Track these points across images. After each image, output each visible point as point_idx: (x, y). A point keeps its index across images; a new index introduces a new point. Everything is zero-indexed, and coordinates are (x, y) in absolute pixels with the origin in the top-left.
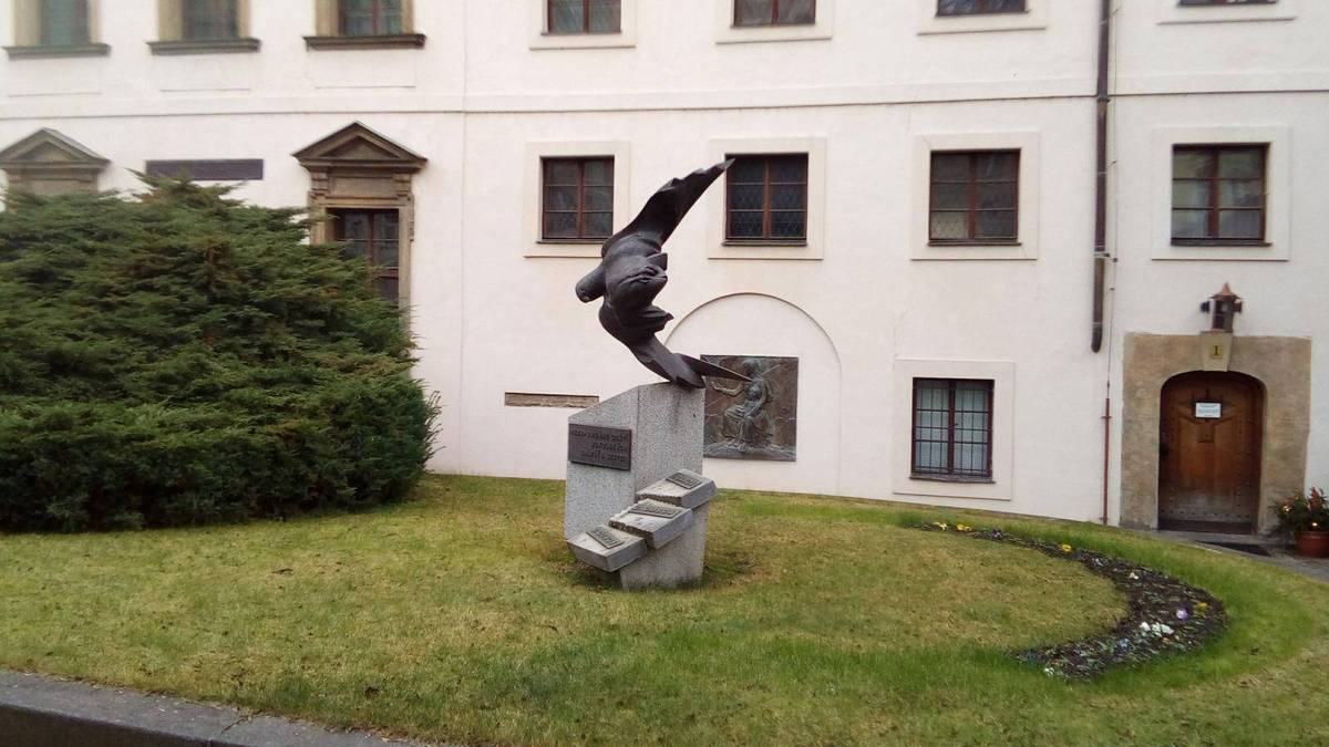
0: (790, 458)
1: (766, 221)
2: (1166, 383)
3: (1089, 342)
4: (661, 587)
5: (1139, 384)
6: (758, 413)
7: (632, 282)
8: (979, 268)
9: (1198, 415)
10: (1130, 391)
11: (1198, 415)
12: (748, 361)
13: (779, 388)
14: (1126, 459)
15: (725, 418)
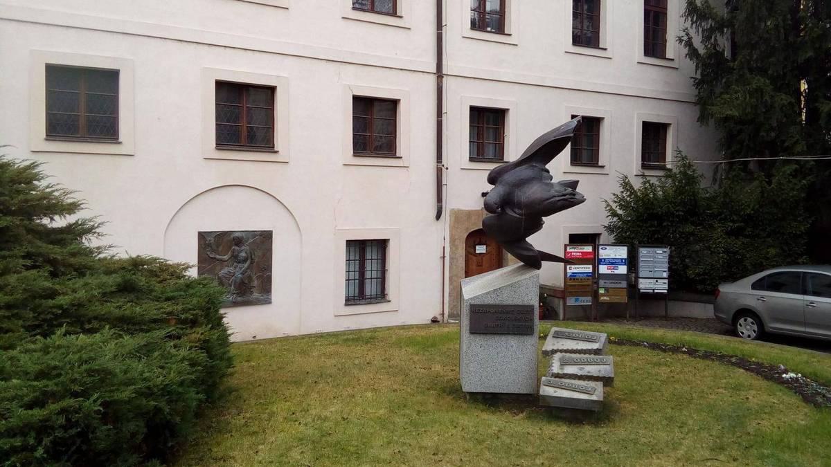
0: (269, 302)
1: (82, 122)
2: (467, 237)
3: (434, 213)
4: (561, 351)
5: (456, 237)
6: (246, 272)
7: (559, 201)
8: (375, 169)
9: (477, 252)
10: (453, 241)
11: (477, 252)
12: (236, 235)
13: (259, 253)
14: (451, 278)
15: (219, 278)
